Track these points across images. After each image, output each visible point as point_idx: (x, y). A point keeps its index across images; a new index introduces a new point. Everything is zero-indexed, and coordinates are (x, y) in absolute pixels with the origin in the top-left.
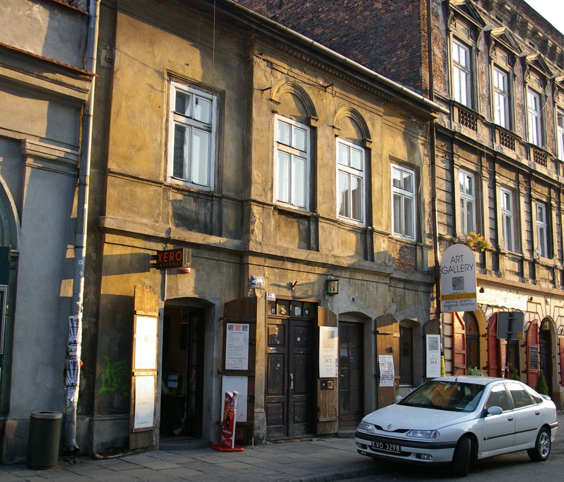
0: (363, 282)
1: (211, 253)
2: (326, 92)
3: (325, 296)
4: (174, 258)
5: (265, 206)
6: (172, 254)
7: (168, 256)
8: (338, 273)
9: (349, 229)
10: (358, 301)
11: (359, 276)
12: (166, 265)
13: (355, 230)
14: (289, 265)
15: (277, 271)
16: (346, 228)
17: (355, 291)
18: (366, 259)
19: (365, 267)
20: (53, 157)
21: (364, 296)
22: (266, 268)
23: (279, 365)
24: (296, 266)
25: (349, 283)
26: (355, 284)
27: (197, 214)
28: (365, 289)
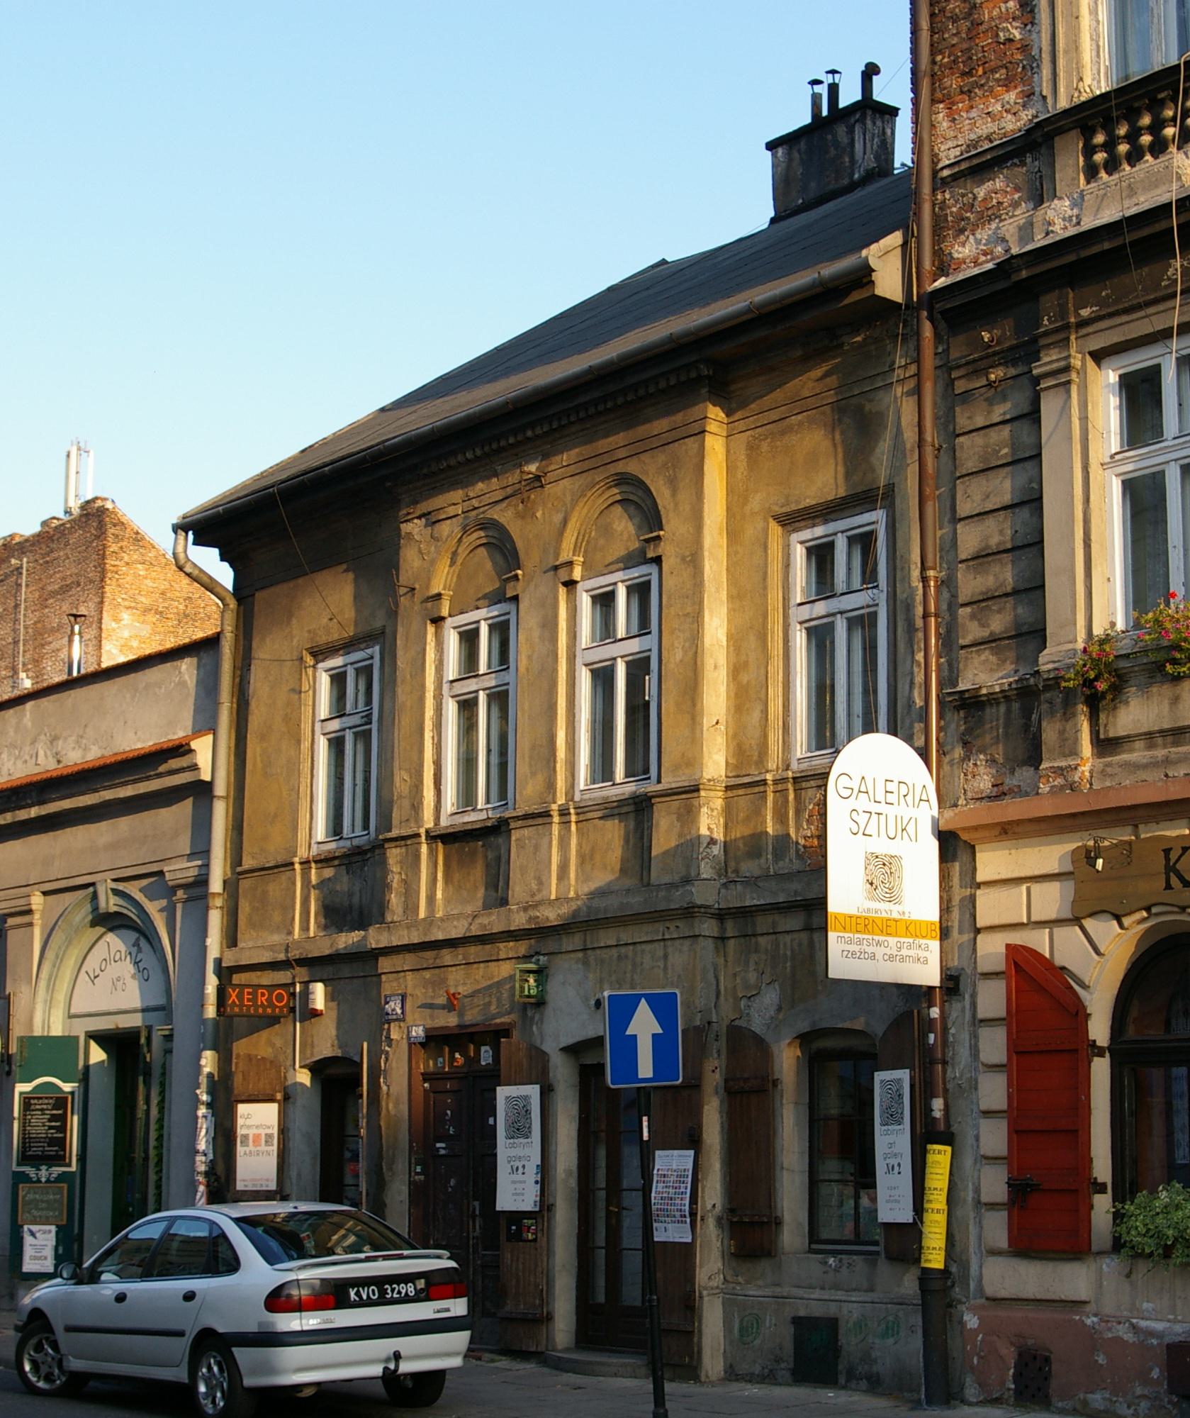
0: (623, 950)
2: (542, 486)
4: (269, 1000)
5: (409, 842)
6: (263, 995)
7: (254, 994)
9: (600, 814)
11: (607, 937)
12: (248, 1010)
13: (616, 811)
14: (447, 957)
15: (427, 974)
16: (590, 815)
17: (601, 981)
19: (606, 911)
20: (191, 880)
22: (410, 975)
23: (452, 1182)
24: (459, 955)
25: (586, 963)
26: (602, 961)
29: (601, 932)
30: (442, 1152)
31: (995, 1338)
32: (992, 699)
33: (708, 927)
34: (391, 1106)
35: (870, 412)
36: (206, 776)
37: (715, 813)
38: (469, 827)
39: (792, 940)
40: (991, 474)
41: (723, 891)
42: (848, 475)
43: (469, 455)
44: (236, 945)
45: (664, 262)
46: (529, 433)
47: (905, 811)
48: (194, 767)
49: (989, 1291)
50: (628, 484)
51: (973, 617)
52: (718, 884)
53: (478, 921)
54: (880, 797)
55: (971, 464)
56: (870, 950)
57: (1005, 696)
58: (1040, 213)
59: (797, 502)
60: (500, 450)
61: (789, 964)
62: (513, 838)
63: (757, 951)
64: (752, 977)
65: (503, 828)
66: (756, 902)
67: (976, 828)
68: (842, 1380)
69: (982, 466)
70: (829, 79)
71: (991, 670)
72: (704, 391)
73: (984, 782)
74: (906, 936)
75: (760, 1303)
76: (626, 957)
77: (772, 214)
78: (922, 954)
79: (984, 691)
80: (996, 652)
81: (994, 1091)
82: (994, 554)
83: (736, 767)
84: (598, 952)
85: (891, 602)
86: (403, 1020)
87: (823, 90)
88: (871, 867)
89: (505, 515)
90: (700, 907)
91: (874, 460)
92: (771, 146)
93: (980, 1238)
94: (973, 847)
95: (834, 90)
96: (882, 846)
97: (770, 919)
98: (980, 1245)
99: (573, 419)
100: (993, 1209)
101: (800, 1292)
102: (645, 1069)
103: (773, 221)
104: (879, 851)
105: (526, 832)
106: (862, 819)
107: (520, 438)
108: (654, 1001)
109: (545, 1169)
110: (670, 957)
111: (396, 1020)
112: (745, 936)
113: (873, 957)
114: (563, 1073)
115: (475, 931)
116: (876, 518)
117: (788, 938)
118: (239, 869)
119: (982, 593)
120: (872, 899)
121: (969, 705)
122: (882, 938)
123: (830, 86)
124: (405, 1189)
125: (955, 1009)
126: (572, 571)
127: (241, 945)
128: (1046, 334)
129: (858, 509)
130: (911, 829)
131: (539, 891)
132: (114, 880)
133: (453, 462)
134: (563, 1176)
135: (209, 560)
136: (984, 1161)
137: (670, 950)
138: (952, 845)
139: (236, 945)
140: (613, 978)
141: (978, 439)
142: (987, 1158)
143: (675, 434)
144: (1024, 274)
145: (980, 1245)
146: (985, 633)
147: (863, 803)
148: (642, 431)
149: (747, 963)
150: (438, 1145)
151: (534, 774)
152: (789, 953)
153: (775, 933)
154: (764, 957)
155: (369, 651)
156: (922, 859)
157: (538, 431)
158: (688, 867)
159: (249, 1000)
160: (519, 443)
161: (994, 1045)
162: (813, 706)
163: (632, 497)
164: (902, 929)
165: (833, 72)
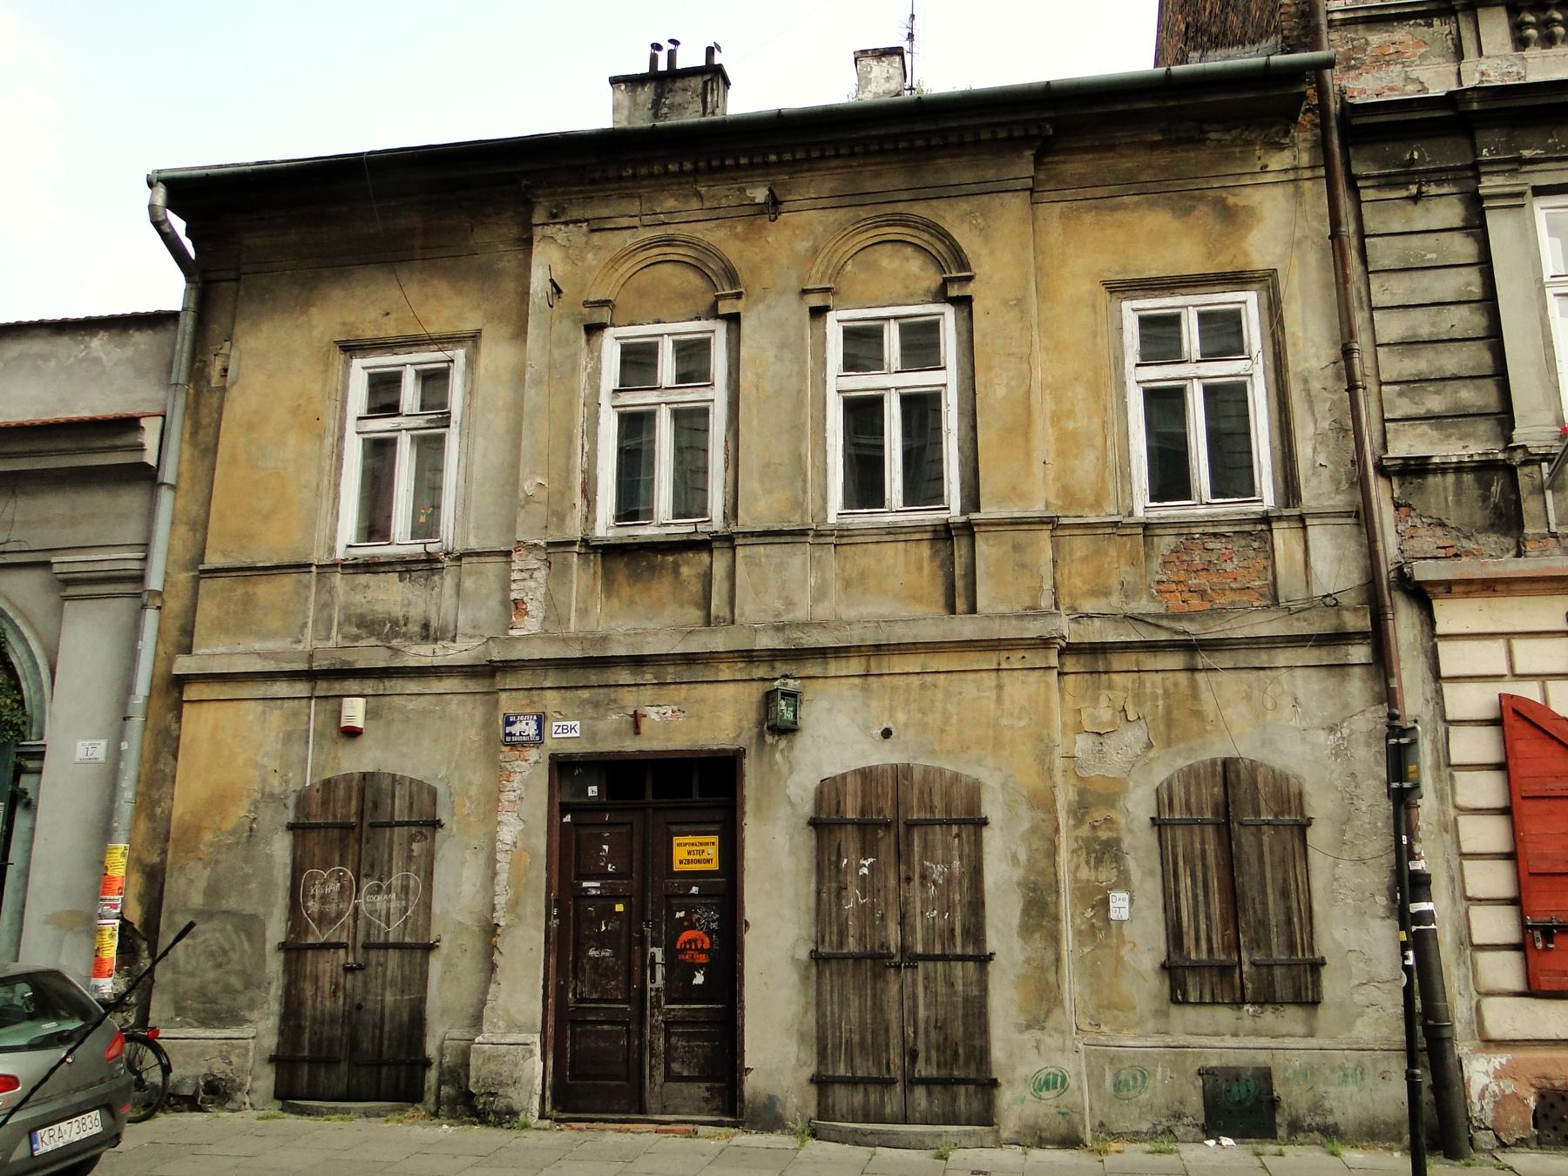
0: (929, 679)
3: (761, 735)
8: (812, 669)
18: (952, 609)
25: (866, 689)
26: (893, 689)
29: (895, 658)
32: (1443, 469)
36: (150, 458)
40: (1415, 274)
48: (140, 448)
51: (1401, 394)
57: (1459, 468)
59: (1137, 271)
63: (1110, 687)
64: (1105, 714)
68: (1282, 1132)
75: (1147, 1054)
79: (1436, 460)
92: (615, 81)
95: (672, 56)
101: (1204, 1041)
116: (1250, 303)
117: (1158, 677)
129: (1217, 288)
140: (914, 706)
143: (983, 187)
144: (1475, 106)
148: (930, 179)
149: (1096, 700)
152: (1160, 692)
165: (675, 42)
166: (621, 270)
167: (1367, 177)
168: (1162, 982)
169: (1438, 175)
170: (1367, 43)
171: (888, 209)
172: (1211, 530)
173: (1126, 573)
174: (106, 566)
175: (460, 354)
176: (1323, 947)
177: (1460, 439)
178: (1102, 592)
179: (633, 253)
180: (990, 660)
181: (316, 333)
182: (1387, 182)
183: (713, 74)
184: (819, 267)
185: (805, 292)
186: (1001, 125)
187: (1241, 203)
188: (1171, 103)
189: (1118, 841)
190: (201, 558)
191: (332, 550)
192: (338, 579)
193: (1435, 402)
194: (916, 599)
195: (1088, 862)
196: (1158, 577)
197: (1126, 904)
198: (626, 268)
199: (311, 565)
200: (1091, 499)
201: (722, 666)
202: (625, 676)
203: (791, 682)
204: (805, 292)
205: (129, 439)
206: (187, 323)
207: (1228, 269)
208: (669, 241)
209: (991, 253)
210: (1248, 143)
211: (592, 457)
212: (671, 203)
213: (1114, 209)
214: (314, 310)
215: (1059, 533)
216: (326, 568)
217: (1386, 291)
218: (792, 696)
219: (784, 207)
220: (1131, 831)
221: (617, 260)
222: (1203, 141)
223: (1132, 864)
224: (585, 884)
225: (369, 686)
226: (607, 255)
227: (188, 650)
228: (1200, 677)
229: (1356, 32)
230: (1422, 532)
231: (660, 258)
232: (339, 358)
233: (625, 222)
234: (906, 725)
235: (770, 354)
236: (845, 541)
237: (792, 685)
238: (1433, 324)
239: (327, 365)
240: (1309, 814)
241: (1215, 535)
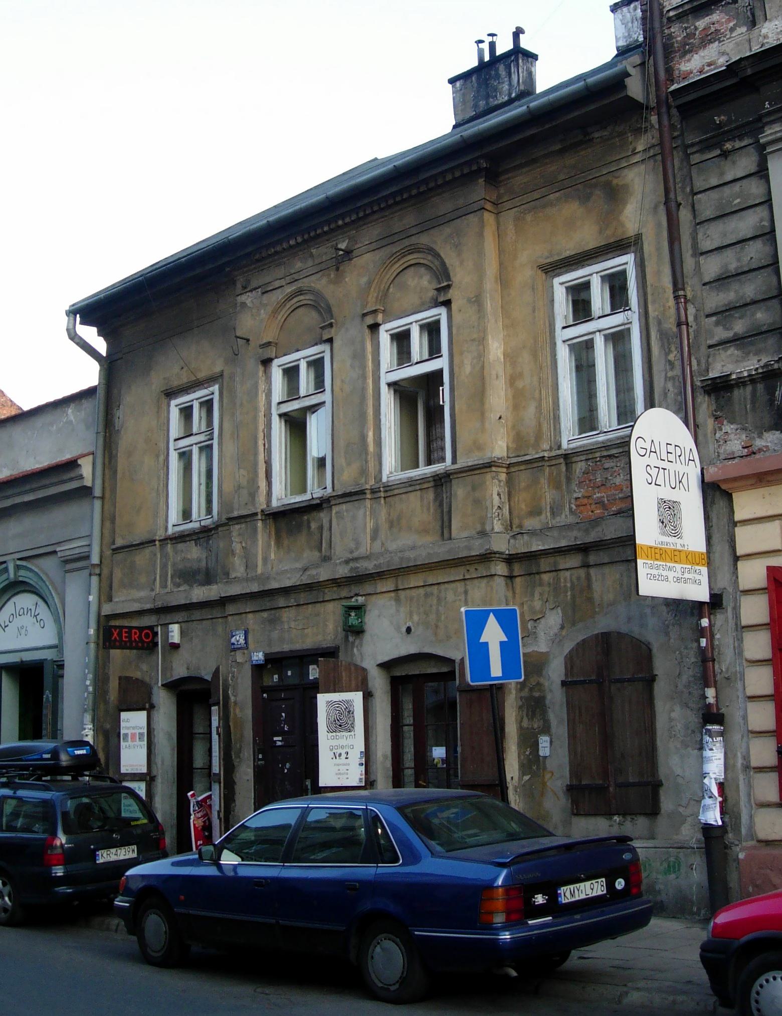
0: (429, 589)
1: (204, 611)
3: (347, 637)
6: (135, 633)
7: (129, 632)
8: (368, 588)
10: (417, 631)
15: (265, 615)
21: (432, 617)
22: (250, 616)
25: (398, 600)
26: (411, 599)
27: (199, 560)
28: (435, 601)
30: (279, 743)
31: (769, 871)
32: (741, 382)
33: (501, 568)
34: (238, 711)
35: (617, 185)
36: (89, 484)
37: (502, 484)
38: (297, 506)
39: (571, 575)
40: (726, 219)
41: (512, 541)
42: (600, 232)
43: (292, 242)
44: (111, 601)
45: (376, 159)
46: (340, 222)
47: (680, 468)
48: (81, 477)
49: (762, 835)
50: (419, 252)
51: (717, 324)
52: (508, 536)
53: (308, 573)
54: (664, 457)
55: (709, 213)
56: (664, 573)
57: (752, 380)
58: (756, 32)
59: (558, 254)
60: (318, 236)
61: (569, 593)
62: (334, 512)
63: (541, 585)
64: (537, 604)
65: (325, 505)
66: (541, 548)
67: (735, 479)
69: (718, 213)
70: (490, 39)
71: (737, 361)
72: (481, 181)
73: (735, 445)
74: (687, 564)
76: (432, 594)
77: (454, 123)
78: (698, 577)
79: (734, 377)
80: (738, 347)
81: (760, 681)
82: (733, 276)
83: (516, 449)
84: (408, 591)
85: (643, 320)
86: (247, 648)
87: (485, 47)
88: (662, 509)
89: (320, 283)
90: (495, 553)
91: (623, 218)
92: (452, 81)
93: (749, 795)
94: (731, 495)
95: (492, 46)
96: (667, 493)
97: (551, 560)
98: (750, 800)
99: (376, 208)
100: (761, 772)
102: (496, 670)
103: (455, 127)
104: (666, 498)
105: (344, 507)
106: (654, 472)
107: (333, 226)
108: (499, 615)
109: (368, 754)
110: (470, 592)
111: (239, 649)
112: (530, 574)
113: (667, 579)
114: (379, 683)
115: (305, 580)
116: (627, 262)
117: (568, 574)
118: (114, 547)
119: (726, 305)
120: (663, 534)
121: (720, 388)
122: (672, 565)
123: (490, 43)
124: (251, 771)
125: (719, 618)
126: (377, 317)
127: (115, 599)
128: (769, 113)
129: (610, 255)
130: (684, 481)
131: (357, 549)
132: (19, 559)
133: (279, 248)
134: (381, 759)
135: (90, 334)
136: (750, 735)
137: (469, 587)
138: (715, 493)
139: (111, 601)
140: (422, 610)
141: (713, 195)
142: (752, 732)
144: (749, 72)
145: (750, 800)
146: (729, 334)
147: (653, 460)
149: (532, 595)
150: (275, 739)
151: (349, 464)
152: (569, 585)
153: (556, 571)
154: (547, 589)
155: (211, 389)
156: (692, 504)
157: (347, 220)
158: (483, 524)
159: (126, 637)
160: (332, 230)
161: (759, 645)
162: (575, 403)
163: (422, 261)
164: (683, 556)
166: (279, 317)
167: (693, 145)
168: (567, 800)
169: (738, 133)
170: (696, 28)
171: (406, 242)
172: (605, 453)
173: (548, 495)
174: (77, 551)
175: (216, 388)
176: (662, 772)
177: (755, 354)
178: (535, 512)
179: (284, 304)
180: (457, 573)
181: (154, 387)
182: (705, 146)
183: (519, 56)
184: (372, 298)
185: (364, 315)
186: (446, 171)
187: (620, 183)
188: (547, 126)
189: (543, 698)
190: (113, 543)
191: (166, 529)
192: (169, 547)
193: (739, 327)
194: (425, 531)
195: (527, 715)
196: (575, 495)
197: (548, 744)
198: (281, 317)
199: (155, 541)
200: (532, 440)
201: (326, 591)
202: (281, 602)
203: (360, 598)
204: (364, 315)
205: (72, 474)
206: (101, 393)
207: (612, 240)
208: (300, 292)
209: (462, 263)
210: (621, 134)
211: (268, 452)
212: (299, 265)
213: (544, 206)
214: (153, 373)
215: (513, 470)
216: (165, 540)
217: (712, 236)
218: (359, 609)
219: (355, 253)
220: (551, 691)
221: (275, 312)
222: (591, 140)
223: (552, 716)
224: (275, 739)
225: (182, 616)
226: (270, 309)
227: (110, 599)
228: (592, 571)
229: (687, 22)
230: (732, 436)
231: (298, 304)
232: (164, 401)
233: (277, 284)
234: (418, 624)
235: (348, 362)
236: (389, 494)
237: (361, 600)
238: (739, 260)
239: (159, 408)
240: (656, 672)
241: (610, 456)
